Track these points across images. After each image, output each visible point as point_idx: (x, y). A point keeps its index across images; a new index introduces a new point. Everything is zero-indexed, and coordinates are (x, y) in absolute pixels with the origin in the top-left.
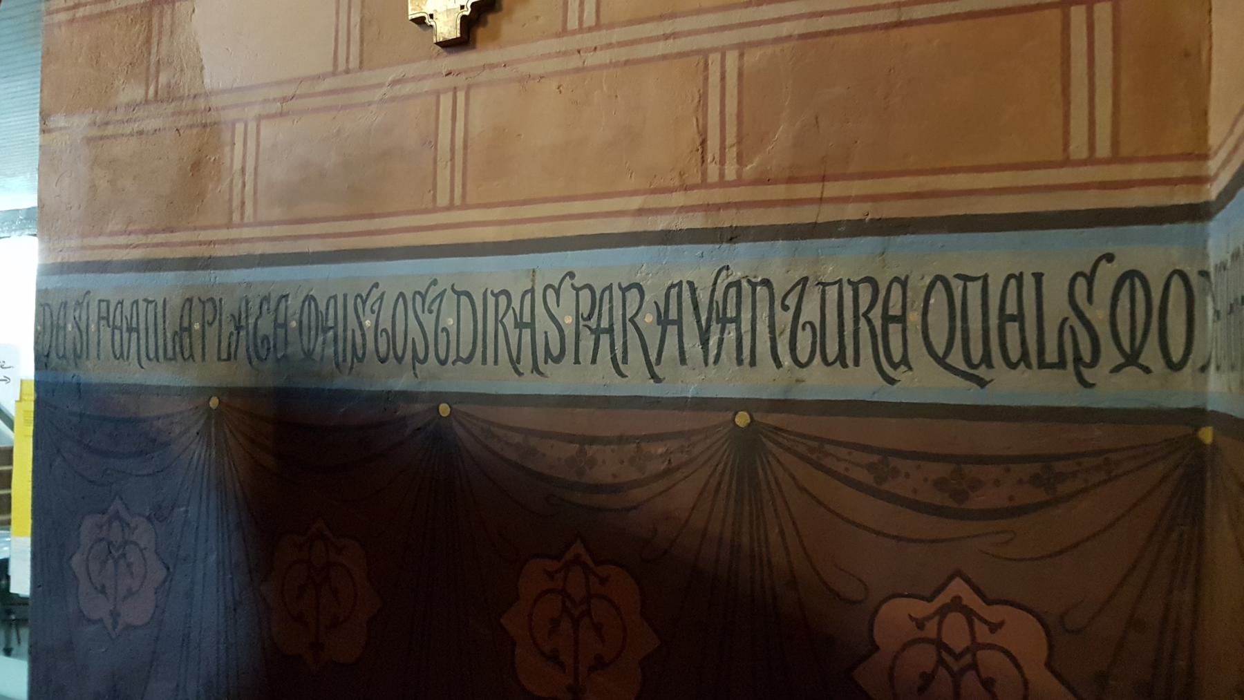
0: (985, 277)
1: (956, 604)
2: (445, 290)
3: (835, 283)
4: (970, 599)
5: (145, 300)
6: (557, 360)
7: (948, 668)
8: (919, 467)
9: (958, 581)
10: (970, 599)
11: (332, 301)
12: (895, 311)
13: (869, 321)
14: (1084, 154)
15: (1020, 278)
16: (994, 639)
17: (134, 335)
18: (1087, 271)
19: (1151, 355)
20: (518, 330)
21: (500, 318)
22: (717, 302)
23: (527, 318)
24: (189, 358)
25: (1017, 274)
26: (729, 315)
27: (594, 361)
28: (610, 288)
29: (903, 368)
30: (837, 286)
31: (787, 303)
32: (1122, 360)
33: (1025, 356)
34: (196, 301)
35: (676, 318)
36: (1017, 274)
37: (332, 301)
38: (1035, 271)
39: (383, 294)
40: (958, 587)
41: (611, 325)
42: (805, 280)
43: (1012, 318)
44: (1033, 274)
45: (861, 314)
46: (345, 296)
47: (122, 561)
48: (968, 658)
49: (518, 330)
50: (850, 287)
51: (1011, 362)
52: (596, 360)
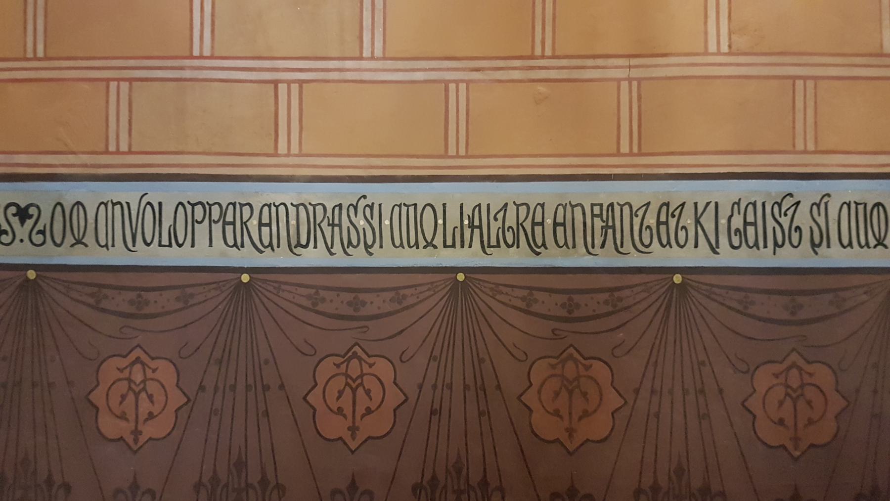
0: (415, 205)
1: (794, 365)
2: (711, 202)
3: (413, 205)
4: (801, 362)
9: (794, 353)
10: (801, 362)
12: (538, 219)
14: (286, 152)
16: (372, 370)
17: (477, 231)
22: (739, 213)
23: (610, 224)
25: (848, 202)
26: (475, 224)
27: (470, 246)
28: (612, 205)
30: (413, 206)
31: (788, 212)
32: (74, 241)
33: (566, 243)
34: (615, 204)
35: (478, 224)
36: (848, 202)
37: (337, 209)
38: (482, 205)
40: (794, 357)
45: (317, 224)
46: (764, 205)
49: (331, 227)
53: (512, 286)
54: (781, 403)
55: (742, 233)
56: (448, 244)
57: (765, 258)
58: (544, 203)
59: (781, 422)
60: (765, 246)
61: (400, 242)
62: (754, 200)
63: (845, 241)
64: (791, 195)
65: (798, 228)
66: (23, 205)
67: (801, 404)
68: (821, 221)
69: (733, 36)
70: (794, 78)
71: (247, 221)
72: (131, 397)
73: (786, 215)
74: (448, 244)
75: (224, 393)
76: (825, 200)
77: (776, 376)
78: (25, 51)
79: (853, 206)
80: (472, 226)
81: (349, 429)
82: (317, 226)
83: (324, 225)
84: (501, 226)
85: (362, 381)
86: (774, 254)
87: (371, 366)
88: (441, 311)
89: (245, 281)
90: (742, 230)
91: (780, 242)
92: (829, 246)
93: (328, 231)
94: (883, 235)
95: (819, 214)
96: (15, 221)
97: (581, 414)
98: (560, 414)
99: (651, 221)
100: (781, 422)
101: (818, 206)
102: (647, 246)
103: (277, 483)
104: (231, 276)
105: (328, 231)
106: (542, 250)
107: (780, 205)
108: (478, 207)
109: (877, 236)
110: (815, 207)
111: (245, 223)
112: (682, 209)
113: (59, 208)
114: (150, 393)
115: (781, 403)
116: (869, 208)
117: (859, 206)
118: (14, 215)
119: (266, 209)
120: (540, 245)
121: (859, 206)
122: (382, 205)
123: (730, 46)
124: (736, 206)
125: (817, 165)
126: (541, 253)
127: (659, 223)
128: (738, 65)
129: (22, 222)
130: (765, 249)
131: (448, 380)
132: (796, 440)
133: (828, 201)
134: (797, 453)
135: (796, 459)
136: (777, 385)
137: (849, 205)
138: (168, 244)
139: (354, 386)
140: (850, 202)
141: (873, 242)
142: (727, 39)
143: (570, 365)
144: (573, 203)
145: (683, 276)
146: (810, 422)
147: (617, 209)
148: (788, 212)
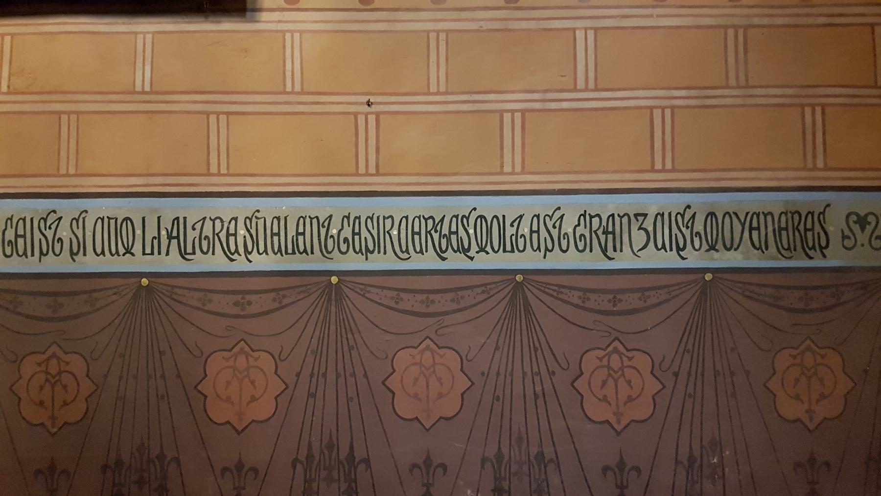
5: (791, 212)
6: (372, 252)
7: (613, 377)
8: (599, 296)
11: (404, 220)
13: (799, 231)
15: (663, 215)
16: (68, 368)
18: (77, 217)
19: (719, 246)
20: (605, 236)
21: (795, 227)
22: (12, 227)
23: (610, 229)
24: (359, 252)
25: (418, 216)
26: (609, 230)
27: (167, 254)
28: (613, 215)
29: (813, 251)
34: (616, 216)
35: (176, 235)
36: (102, 217)
39: (562, 217)
40: (54, 349)
41: (272, 238)
42: (204, 218)
43: (232, 235)
44: (237, 217)
46: (32, 219)
47: (621, 380)
48: (57, 378)
49: (605, 236)
50: (310, 219)
51: (328, 251)
52: (672, 248)
53: (762, 285)
54: (42, 388)
55: (13, 244)
56: (147, 252)
57: (32, 265)
58: (408, 215)
59: (41, 403)
60: (33, 255)
61: (303, 248)
62: (24, 216)
63: (99, 251)
64: (54, 211)
65: (60, 239)
66: (862, 214)
67: (622, 383)
68: (80, 234)
69: (12, 78)
70: (59, 113)
71: (220, 232)
72: (611, 382)
73: (50, 228)
74: (146, 252)
75: (318, 378)
76: (83, 215)
77: (39, 364)
78: (285, 86)
79: (106, 220)
80: (170, 237)
81: (807, 412)
82: (386, 233)
83: (600, 232)
84: (515, 233)
85: (434, 369)
86: (40, 261)
87: (441, 356)
88: (506, 308)
89: (706, 278)
90: (13, 240)
91: (45, 251)
92: (85, 254)
93: (602, 238)
94: (130, 245)
95: (78, 228)
96: (856, 228)
97: (249, 399)
98: (419, 397)
99: (445, 231)
100: (41, 403)
101: (77, 221)
102: (330, 253)
103: (297, 457)
104: (134, 280)
105: (602, 238)
106: (406, 256)
107: (45, 220)
108: (611, 218)
109: (126, 246)
110: (74, 221)
111: (217, 234)
112: (330, 220)
113: (495, 220)
114: (627, 379)
115: (42, 388)
116: (119, 222)
117: (111, 221)
118: (855, 222)
119: (417, 220)
120: (301, 251)
121: (111, 221)
122: (146, 218)
123: (9, 87)
124: (9, 221)
125: (76, 186)
126: (447, 258)
127: (532, 232)
128: (14, 102)
129: (863, 229)
130: (33, 257)
131: (323, 370)
132: (53, 418)
133: (86, 216)
134: (55, 430)
135: (54, 435)
136: (39, 372)
137: (103, 219)
138: (150, 252)
139: (616, 376)
140: (103, 217)
141: (122, 250)
142: (7, 80)
143: (615, 357)
144: (213, 218)
145: (341, 278)
146: (65, 404)
147: (617, 219)
148: (52, 226)
